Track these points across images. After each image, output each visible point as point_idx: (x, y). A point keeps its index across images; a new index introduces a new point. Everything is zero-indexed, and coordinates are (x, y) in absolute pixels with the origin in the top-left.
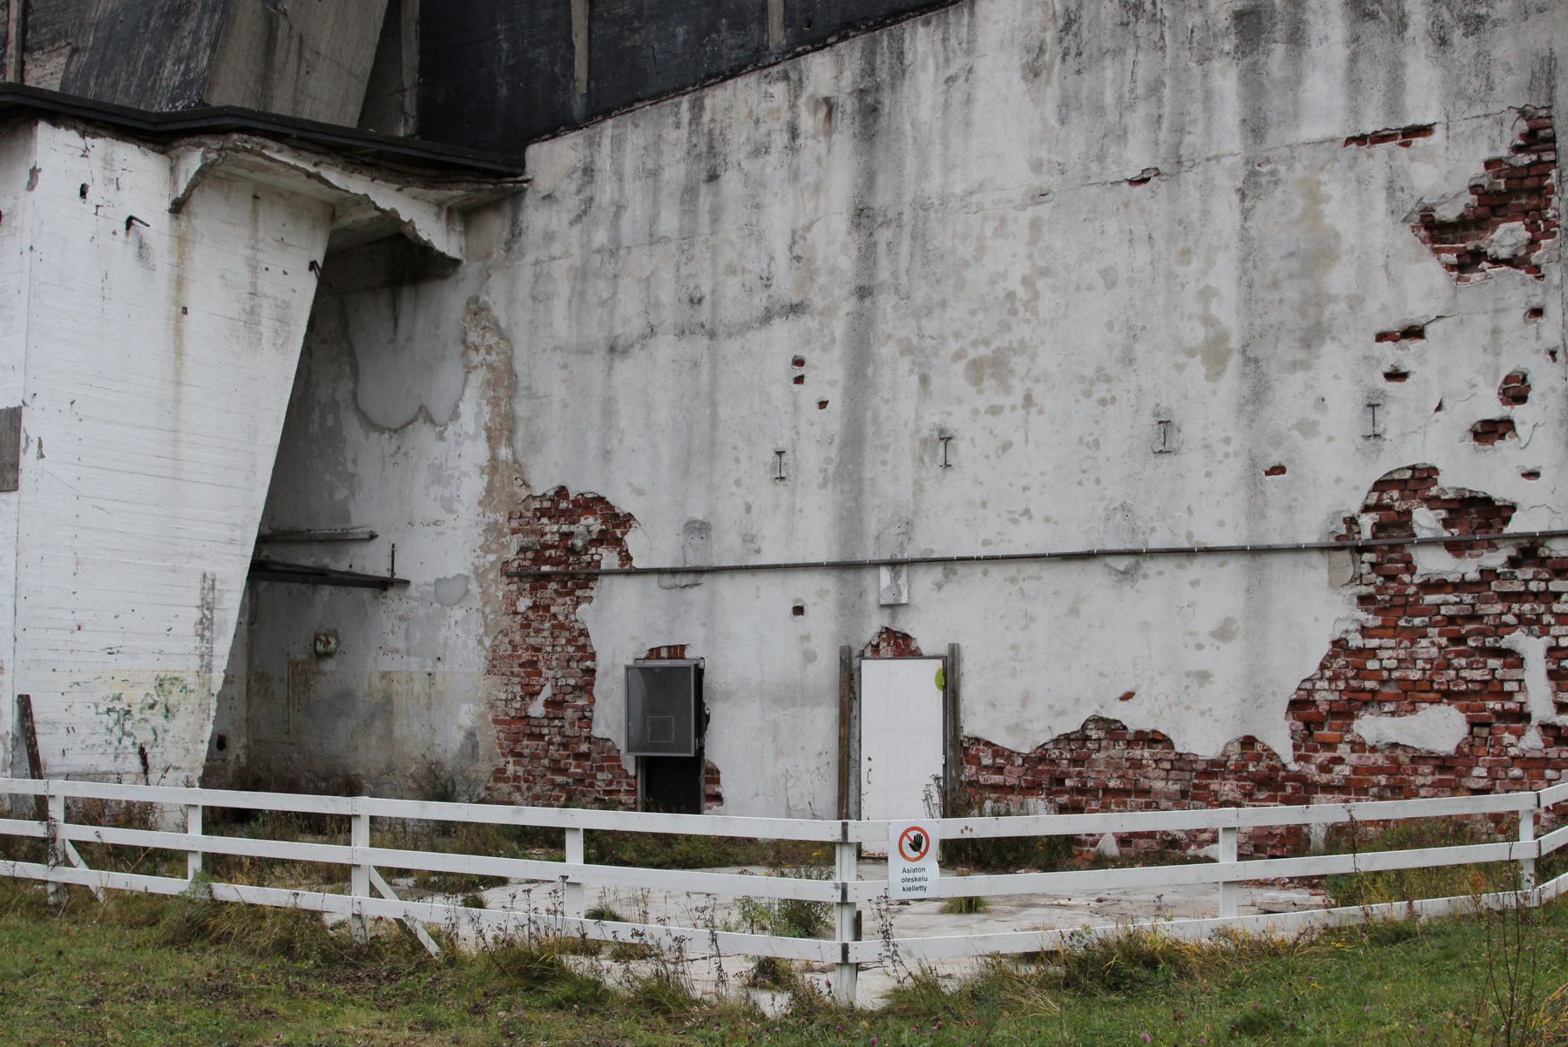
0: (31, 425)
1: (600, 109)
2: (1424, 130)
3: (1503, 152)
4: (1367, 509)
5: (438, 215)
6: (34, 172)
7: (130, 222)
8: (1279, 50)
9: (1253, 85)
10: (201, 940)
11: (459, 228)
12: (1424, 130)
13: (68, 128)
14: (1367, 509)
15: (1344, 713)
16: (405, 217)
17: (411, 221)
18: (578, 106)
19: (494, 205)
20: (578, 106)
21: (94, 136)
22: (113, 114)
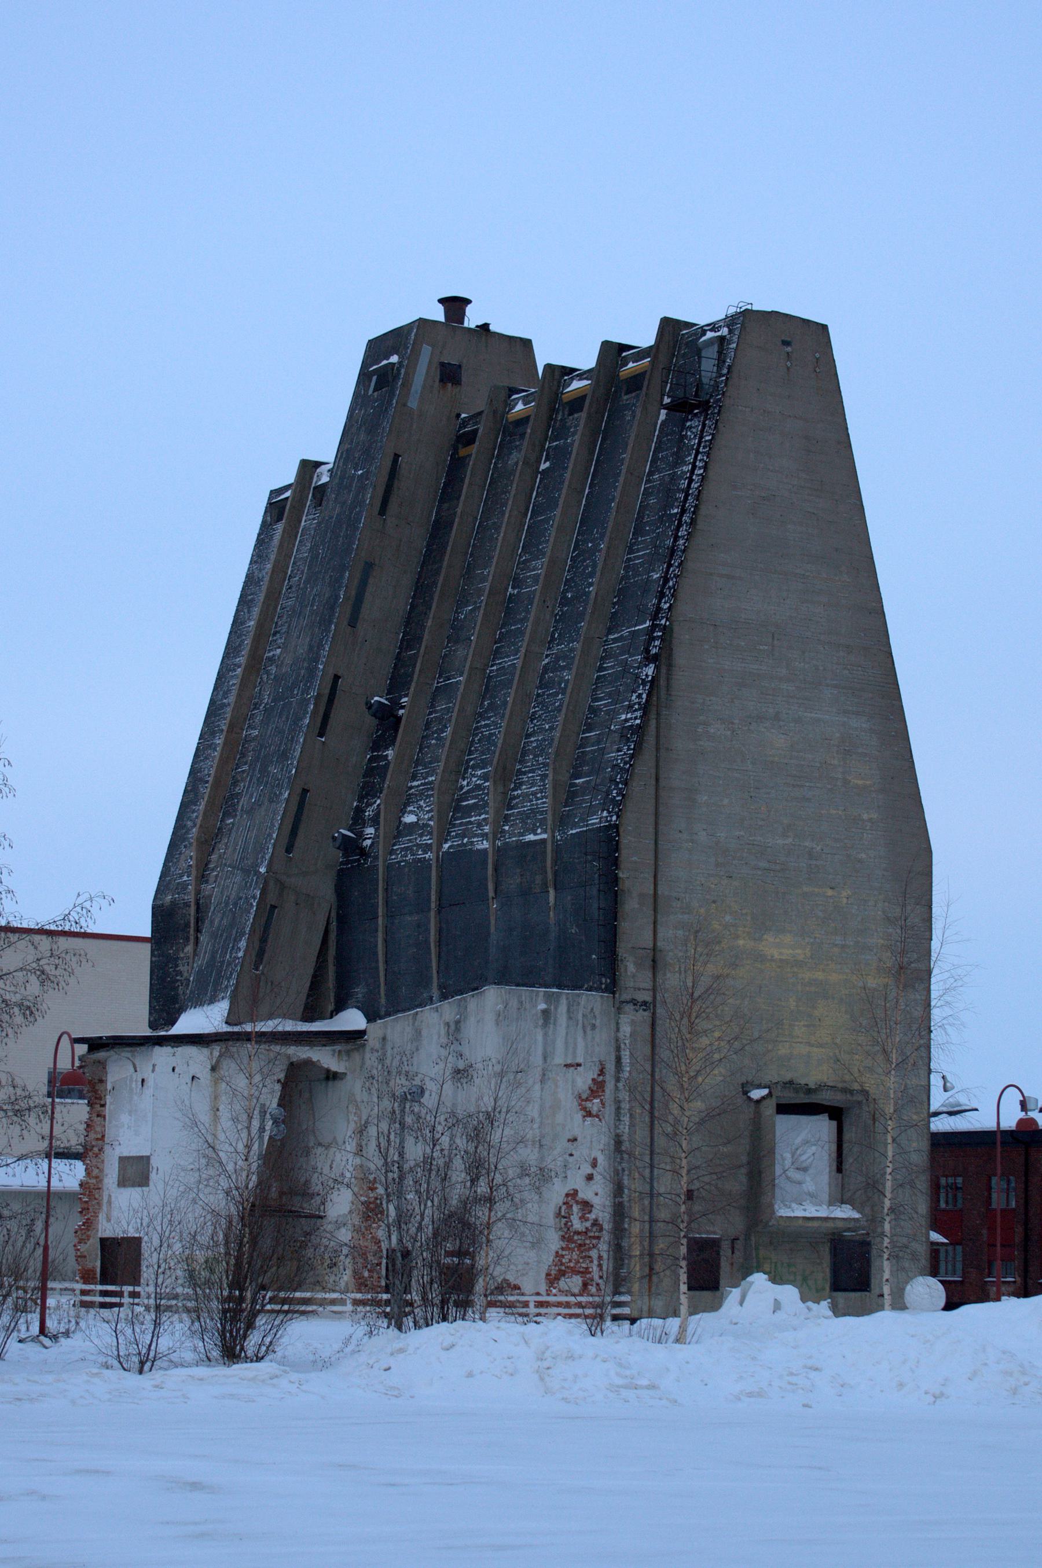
0: (154, 1162)
1: (388, 1014)
2: (579, 1065)
3: (595, 1077)
4: (564, 1204)
5: (333, 1055)
6: (154, 1066)
7: (193, 1078)
8: (551, 1026)
9: (545, 1035)
10: (604, 1168)
11: (345, 1058)
12: (579, 1065)
13: (167, 1046)
14: (564, 1204)
15: (557, 1279)
16: (315, 1059)
17: (318, 1061)
18: (382, 1013)
19: (357, 1049)
20: (382, 1013)
21: (177, 1047)
22: (658, 737)
